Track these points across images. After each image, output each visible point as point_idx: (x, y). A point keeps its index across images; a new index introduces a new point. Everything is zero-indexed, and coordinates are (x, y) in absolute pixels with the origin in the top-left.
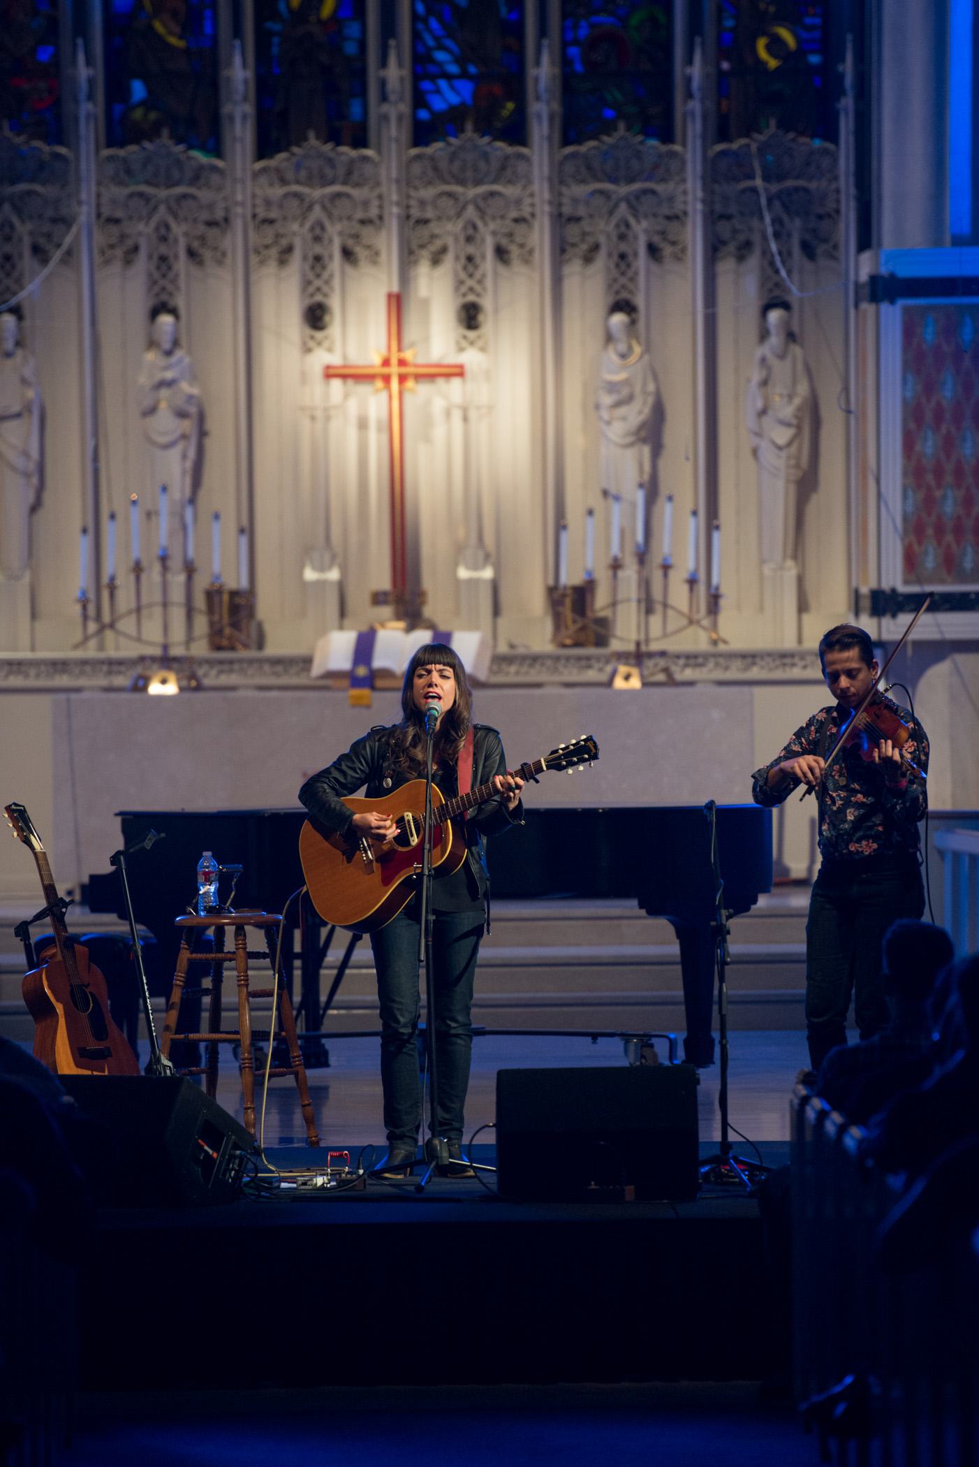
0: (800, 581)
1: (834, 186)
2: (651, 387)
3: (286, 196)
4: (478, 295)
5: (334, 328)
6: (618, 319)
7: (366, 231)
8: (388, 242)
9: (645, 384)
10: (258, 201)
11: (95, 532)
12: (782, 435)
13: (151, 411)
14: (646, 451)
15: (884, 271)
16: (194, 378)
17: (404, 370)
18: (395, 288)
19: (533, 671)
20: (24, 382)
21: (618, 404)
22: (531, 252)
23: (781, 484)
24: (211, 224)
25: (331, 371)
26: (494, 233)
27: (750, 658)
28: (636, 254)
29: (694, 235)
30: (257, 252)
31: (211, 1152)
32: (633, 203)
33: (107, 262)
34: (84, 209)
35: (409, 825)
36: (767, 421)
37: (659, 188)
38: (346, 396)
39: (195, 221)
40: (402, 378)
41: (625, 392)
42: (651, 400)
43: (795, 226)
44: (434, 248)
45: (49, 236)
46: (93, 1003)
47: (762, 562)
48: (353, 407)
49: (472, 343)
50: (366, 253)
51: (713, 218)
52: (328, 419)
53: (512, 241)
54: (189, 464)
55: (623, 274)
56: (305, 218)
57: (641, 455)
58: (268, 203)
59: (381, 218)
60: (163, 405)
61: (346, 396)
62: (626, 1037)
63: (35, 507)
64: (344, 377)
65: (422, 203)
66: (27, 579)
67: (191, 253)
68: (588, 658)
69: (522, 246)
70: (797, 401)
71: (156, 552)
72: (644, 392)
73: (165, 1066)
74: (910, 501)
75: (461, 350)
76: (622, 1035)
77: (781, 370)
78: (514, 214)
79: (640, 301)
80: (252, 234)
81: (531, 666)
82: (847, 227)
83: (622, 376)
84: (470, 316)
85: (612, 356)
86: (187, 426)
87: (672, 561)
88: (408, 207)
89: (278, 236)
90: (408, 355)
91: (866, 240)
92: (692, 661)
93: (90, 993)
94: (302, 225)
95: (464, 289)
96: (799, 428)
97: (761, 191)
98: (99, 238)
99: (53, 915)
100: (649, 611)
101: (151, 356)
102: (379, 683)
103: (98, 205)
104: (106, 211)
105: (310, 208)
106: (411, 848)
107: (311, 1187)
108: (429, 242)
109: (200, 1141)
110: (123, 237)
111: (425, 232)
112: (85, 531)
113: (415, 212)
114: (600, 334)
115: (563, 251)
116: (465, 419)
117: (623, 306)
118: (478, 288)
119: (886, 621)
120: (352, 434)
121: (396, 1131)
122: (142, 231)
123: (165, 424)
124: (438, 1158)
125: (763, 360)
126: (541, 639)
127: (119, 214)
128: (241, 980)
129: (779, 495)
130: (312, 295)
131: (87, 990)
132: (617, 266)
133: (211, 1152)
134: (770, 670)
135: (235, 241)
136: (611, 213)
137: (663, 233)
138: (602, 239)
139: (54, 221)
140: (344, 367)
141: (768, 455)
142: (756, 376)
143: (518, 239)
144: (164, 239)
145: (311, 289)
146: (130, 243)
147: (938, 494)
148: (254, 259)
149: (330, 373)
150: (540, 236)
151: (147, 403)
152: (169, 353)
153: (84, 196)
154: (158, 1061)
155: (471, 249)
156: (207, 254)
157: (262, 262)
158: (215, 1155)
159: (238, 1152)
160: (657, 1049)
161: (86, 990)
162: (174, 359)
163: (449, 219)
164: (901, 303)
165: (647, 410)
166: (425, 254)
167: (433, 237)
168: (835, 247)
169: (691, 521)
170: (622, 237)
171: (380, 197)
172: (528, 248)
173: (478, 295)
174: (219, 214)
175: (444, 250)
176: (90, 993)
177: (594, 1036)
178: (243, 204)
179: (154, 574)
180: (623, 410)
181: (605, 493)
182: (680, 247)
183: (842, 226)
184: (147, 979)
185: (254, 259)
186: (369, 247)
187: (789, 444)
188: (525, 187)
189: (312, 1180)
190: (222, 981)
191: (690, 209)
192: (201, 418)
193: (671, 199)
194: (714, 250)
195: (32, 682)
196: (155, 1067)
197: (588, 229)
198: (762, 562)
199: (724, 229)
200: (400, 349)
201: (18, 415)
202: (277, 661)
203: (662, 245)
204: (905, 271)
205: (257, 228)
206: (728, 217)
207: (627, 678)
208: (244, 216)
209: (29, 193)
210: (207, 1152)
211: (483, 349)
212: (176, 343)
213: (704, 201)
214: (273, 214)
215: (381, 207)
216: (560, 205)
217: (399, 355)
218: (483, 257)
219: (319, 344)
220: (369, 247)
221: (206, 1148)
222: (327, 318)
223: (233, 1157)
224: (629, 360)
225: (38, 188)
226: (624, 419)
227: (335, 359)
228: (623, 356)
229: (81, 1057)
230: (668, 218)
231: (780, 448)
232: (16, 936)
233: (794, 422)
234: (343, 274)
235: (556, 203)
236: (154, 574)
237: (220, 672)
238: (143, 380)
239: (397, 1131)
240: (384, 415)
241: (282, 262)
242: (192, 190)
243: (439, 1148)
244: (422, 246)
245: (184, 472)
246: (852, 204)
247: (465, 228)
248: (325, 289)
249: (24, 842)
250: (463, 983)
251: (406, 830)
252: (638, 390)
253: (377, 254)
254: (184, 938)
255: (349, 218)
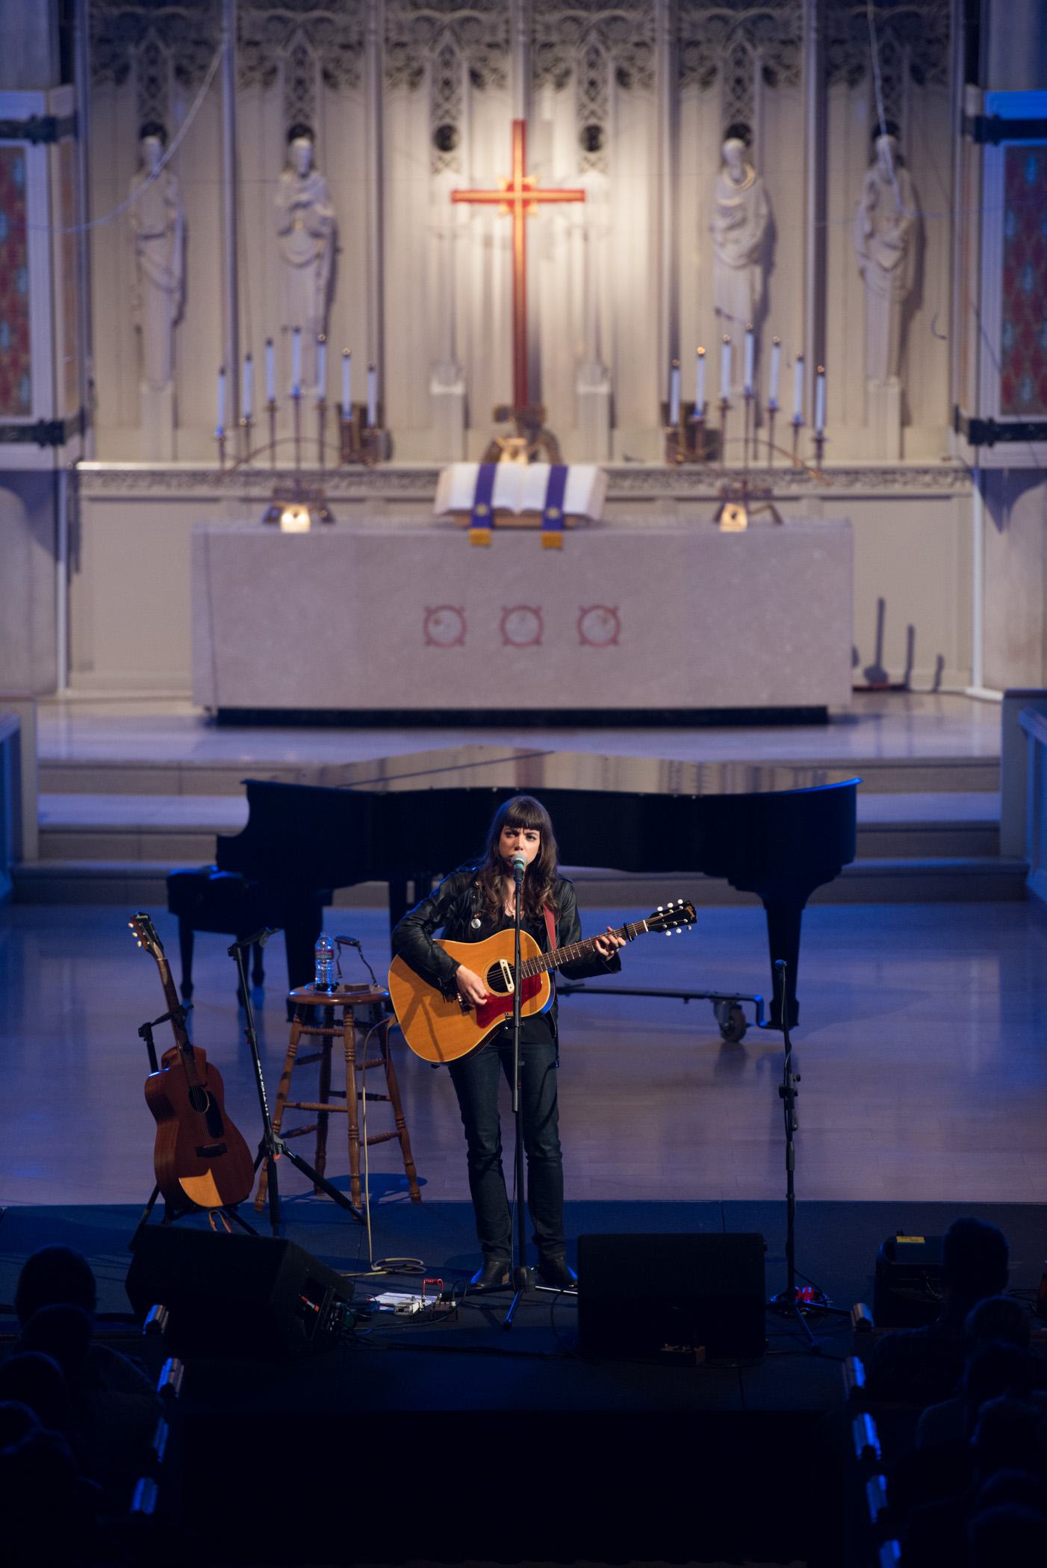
0: (904, 397)
1: (944, 12)
2: (764, 210)
3: (418, 19)
4: (600, 118)
5: (462, 151)
6: (734, 145)
7: (494, 55)
8: (513, 66)
9: (757, 206)
10: (391, 26)
11: (232, 370)
12: (888, 258)
13: (287, 231)
14: (758, 271)
15: (989, 112)
16: (328, 197)
17: (527, 195)
18: (520, 116)
19: (646, 485)
20: (168, 203)
21: (731, 227)
22: (651, 76)
23: (886, 305)
24: (346, 47)
25: (459, 196)
26: (615, 58)
27: (853, 474)
28: (751, 79)
29: (807, 61)
30: (390, 75)
31: (313, 1306)
32: (751, 29)
33: (247, 84)
34: (226, 36)
35: (506, 972)
36: (874, 243)
37: (776, 13)
38: (472, 216)
39: (331, 43)
40: (526, 203)
41: (739, 216)
42: (763, 223)
43: (906, 53)
44: (557, 71)
45: (192, 58)
46: (210, 1103)
47: (867, 377)
48: (478, 227)
49: (593, 165)
50: (494, 76)
51: (827, 43)
52: (454, 237)
53: (633, 65)
54: (323, 282)
55: (739, 98)
56: (435, 41)
57: (752, 275)
58: (400, 27)
59: (507, 41)
60: (299, 226)
61: (472, 216)
62: (716, 999)
63: (177, 321)
64: (471, 201)
65: (548, 28)
66: (169, 390)
67: (327, 76)
68: (698, 474)
69: (641, 70)
70: (904, 225)
71: (290, 391)
72: (757, 215)
73: (277, 1144)
74: (1009, 335)
75: (582, 171)
76: (711, 997)
77: (891, 195)
78: (635, 38)
79: (754, 124)
80: (384, 57)
81: (645, 480)
82: (956, 52)
83: (735, 201)
84: (592, 139)
85: (726, 180)
86: (321, 245)
87: (780, 404)
88: (534, 31)
89: (410, 59)
90: (530, 180)
91: (974, 74)
92: (798, 477)
93: (208, 1092)
94: (432, 49)
95: (586, 113)
96: (905, 250)
97: (870, 16)
98: (239, 61)
99: (174, 1021)
100: (758, 424)
101: (287, 178)
102: (499, 521)
103: (239, 29)
104: (246, 34)
105: (440, 32)
106: (509, 994)
107: (407, 1314)
108: (554, 65)
109: (303, 1298)
110: (262, 59)
111: (549, 55)
112: (223, 372)
113: (541, 37)
114: (716, 160)
115: (682, 75)
116: (586, 238)
117: (737, 131)
118: (599, 112)
119: (984, 450)
120: (478, 252)
121: (489, 1243)
122: (281, 55)
123: (300, 244)
124: (524, 1286)
125: (872, 186)
126: (655, 457)
127: (258, 37)
128: (348, 1056)
129: (884, 315)
130: (442, 118)
131: (205, 1090)
132: (733, 90)
133: (313, 1306)
134: (873, 486)
135: (367, 65)
136: (729, 38)
137: (778, 57)
138: (720, 65)
139: (198, 43)
140: (472, 191)
141: (874, 276)
142: (865, 201)
143: (639, 63)
144: (300, 63)
145: (440, 112)
146: (268, 65)
147: (1036, 328)
148: (386, 82)
149: (456, 198)
150: (660, 61)
151: (284, 223)
152: (304, 176)
153: (225, 24)
154: (271, 1140)
155: (593, 74)
156: (342, 78)
157: (394, 85)
158: (317, 1308)
159: (339, 1304)
160: (744, 1010)
161: (203, 1089)
162: (309, 182)
163: (573, 43)
164: (1005, 144)
165: (759, 233)
166: (549, 78)
167: (558, 60)
168: (944, 71)
169: (797, 368)
170: (739, 63)
171: (507, 22)
172: (648, 73)
173: (600, 118)
174: (354, 38)
175: (567, 73)
176: (208, 1092)
177: (687, 997)
178: (376, 32)
179: (286, 409)
180: (734, 234)
181: (718, 312)
182: (794, 71)
183: (951, 51)
184: (261, 1063)
185: (386, 82)
186: (495, 70)
187: (895, 266)
188: (646, 12)
189: (408, 1307)
190: (331, 1046)
191: (804, 34)
192: (335, 235)
193: (786, 24)
194: (826, 75)
195: (173, 492)
196: (268, 1146)
197: (706, 53)
198: (867, 377)
199: (837, 53)
200: (524, 174)
201: (161, 235)
202: (405, 475)
203: (777, 68)
204: (1009, 113)
205: (390, 52)
206: (841, 42)
207: (734, 516)
208: (377, 45)
209: (174, 16)
210: (310, 1307)
211: (603, 171)
212: (311, 166)
213: (818, 31)
214: (405, 38)
215: (508, 31)
216: (680, 30)
217: (523, 181)
218: (605, 82)
219: (447, 165)
220: (495, 70)
221: (309, 1303)
222: (455, 138)
223: (333, 1308)
224: (743, 185)
225: (181, 10)
226: (737, 241)
227: (462, 183)
228: (737, 181)
229: (198, 1155)
230: (784, 43)
231: (886, 270)
232: (140, 1036)
233: (900, 245)
234: (471, 98)
235: (676, 31)
236: (286, 409)
237: (350, 485)
238: (280, 201)
239: (490, 1243)
240: (508, 233)
241: (413, 85)
242: (327, 14)
243: (526, 1275)
244: (547, 70)
245: (318, 290)
246: (961, 33)
247: (588, 53)
248: (454, 112)
249: (148, 950)
250: (549, 1127)
251: (503, 976)
252: (750, 213)
253: (503, 77)
254: (296, 1012)
255: (478, 42)
